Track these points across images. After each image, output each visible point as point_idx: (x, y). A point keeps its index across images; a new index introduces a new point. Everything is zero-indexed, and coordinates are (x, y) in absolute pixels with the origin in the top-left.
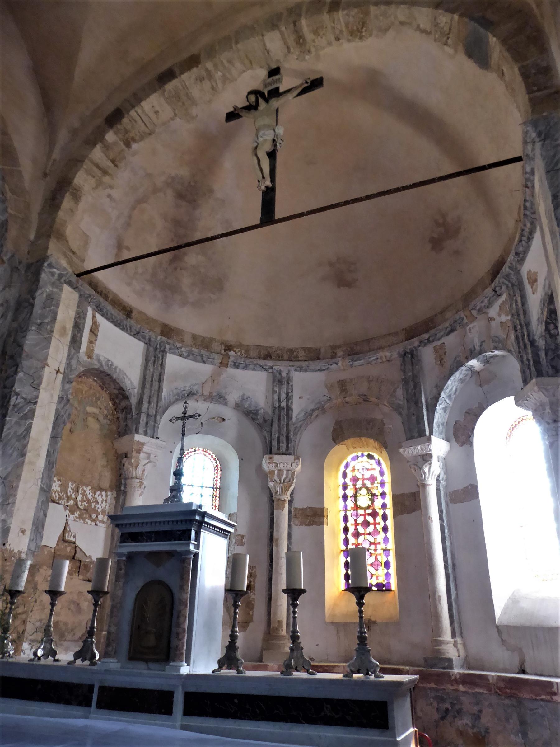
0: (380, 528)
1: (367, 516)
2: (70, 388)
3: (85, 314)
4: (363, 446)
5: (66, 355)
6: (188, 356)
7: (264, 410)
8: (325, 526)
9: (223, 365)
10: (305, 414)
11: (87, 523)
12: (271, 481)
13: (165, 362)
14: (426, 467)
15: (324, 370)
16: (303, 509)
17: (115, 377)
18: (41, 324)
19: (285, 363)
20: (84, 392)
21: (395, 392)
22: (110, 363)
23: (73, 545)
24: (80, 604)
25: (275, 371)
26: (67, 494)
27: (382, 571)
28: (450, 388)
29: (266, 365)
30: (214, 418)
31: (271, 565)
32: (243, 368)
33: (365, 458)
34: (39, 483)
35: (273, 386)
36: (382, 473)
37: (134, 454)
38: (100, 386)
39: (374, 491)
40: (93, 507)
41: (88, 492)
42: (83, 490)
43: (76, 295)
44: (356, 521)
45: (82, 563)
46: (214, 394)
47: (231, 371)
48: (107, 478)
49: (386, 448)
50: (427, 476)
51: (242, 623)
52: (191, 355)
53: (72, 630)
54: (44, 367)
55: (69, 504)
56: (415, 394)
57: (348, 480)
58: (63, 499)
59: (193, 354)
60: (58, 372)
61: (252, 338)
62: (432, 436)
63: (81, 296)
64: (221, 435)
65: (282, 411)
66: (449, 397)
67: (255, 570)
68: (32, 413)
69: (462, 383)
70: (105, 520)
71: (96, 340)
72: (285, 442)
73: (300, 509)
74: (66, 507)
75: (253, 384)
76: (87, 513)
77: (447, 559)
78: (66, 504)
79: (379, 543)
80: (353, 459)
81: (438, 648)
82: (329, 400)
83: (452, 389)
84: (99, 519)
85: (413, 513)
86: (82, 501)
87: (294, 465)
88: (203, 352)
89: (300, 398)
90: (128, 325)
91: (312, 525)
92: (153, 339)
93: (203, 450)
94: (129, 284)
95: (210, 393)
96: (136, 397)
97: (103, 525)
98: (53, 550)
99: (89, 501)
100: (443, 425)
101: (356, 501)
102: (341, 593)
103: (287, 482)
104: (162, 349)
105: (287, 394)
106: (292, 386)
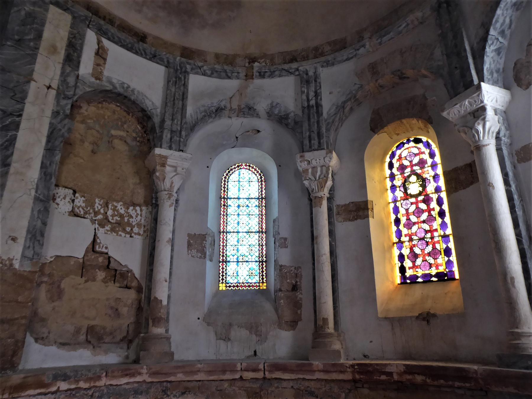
0: (435, 213)
1: (426, 208)
2: (67, 104)
3: (83, 37)
4: (408, 131)
5: (59, 72)
6: (212, 73)
7: (294, 113)
8: (371, 219)
9: (249, 77)
10: (337, 108)
11: (121, 235)
12: (305, 180)
13: (188, 82)
14: (479, 124)
15: (352, 58)
16: (345, 205)
17: (132, 98)
18: (19, 40)
19: (310, 62)
20: (106, 117)
21: (432, 54)
22: (126, 86)
23: (106, 256)
24: (119, 310)
25: (301, 73)
26: (94, 209)
27: (442, 260)
28: (501, 20)
29: (291, 68)
30: (248, 131)
31: (314, 264)
32: (269, 77)
33: (412, 144)
34: (33, 192)
35: (301, 87)
36: (432, 155)
37: (158, 167)
38: (125, 111)
39: (425, 176)
40: (126, 221)
41: (119, 207)
42: (113, 205)
43: (67, 18)
44: (407, 210)
45: (118, 272)
46: (243, 106)
47: (258, 82)
48: (140, 194)
49: (431, 123)
50: (481, 135)
51: (291, 322)
52: (215, 73)
53: (111, 334)
54: (29, 82)
55: (97, 218)
56: (456, 46)
57: (395, 171)
58: (90, 213)
59: (217, 71)
60: (49, 87)
61: (275, 47)
62: (482, 84)
63: (74, 18)
64: (257, 146)
65: (312, 109)
66: (502, 33)
67: (300, 270)
68: (17, 126)
69: (517, 10)
70: (142, 232)
71: (105, 64)
72: (316, 138)
73: (342, 206)
74: (93, 222)
75: (281, 91)
76: (120, 226)
77: (520, 231)
78: (94, 218)
79: (436, 230)
80: (398, 147)
81: (518, 342)
82: (361, 87)
83: (504, 21)
84: (135, 232)
85: (471, 187)
86: (113, 216)
87: (327, 159)
88: (226, 67)
89: (330, 93)
90: (141, 48)
91: (356, 219)
92: (171, 61)
93: (246, 165)
94: (140, 11)
95: (239, 106)
96: (159, 117)
97: (140, 237)
98: (81, 261)
99: (121, 216)
100: (498, 71)
101: (406, 189)
102: (396, 287)
103: (322, 178)
104: (183, 70)
105: (316, 92)
106: (320, 83)
